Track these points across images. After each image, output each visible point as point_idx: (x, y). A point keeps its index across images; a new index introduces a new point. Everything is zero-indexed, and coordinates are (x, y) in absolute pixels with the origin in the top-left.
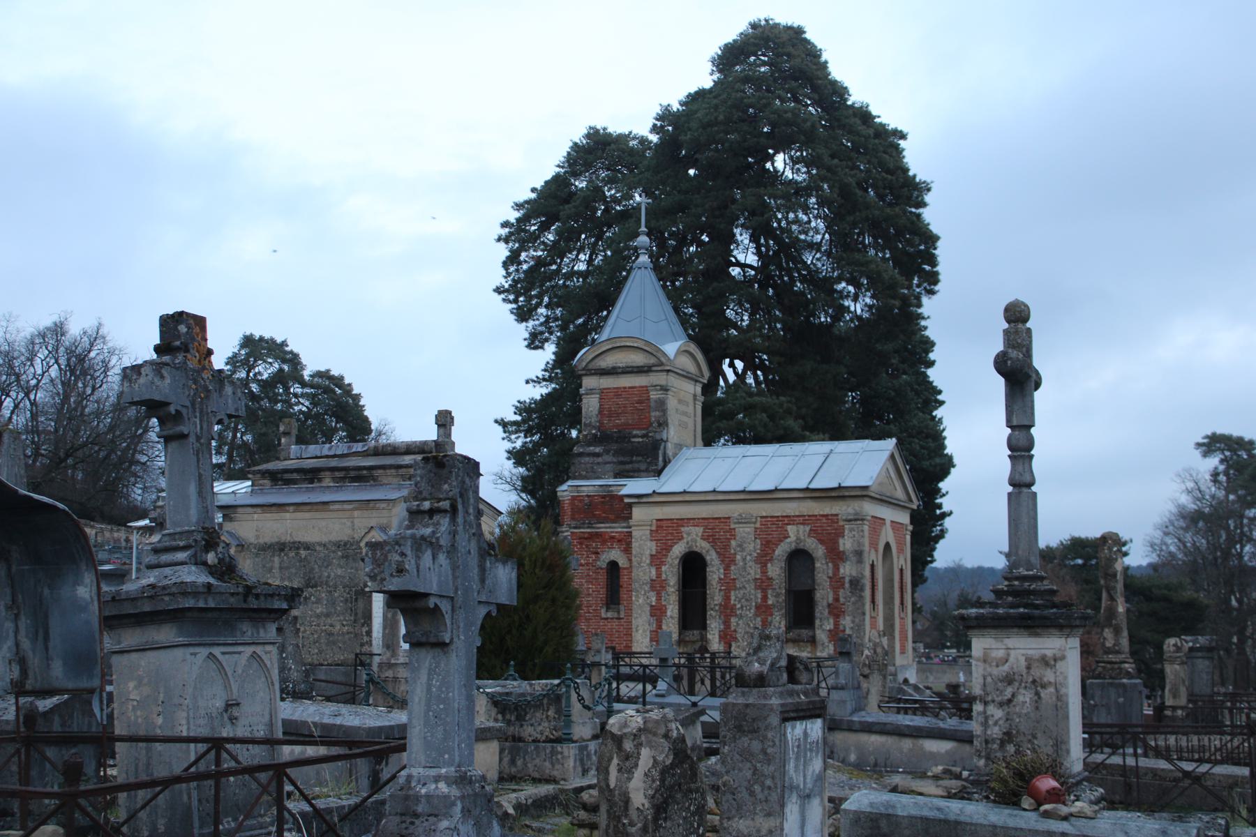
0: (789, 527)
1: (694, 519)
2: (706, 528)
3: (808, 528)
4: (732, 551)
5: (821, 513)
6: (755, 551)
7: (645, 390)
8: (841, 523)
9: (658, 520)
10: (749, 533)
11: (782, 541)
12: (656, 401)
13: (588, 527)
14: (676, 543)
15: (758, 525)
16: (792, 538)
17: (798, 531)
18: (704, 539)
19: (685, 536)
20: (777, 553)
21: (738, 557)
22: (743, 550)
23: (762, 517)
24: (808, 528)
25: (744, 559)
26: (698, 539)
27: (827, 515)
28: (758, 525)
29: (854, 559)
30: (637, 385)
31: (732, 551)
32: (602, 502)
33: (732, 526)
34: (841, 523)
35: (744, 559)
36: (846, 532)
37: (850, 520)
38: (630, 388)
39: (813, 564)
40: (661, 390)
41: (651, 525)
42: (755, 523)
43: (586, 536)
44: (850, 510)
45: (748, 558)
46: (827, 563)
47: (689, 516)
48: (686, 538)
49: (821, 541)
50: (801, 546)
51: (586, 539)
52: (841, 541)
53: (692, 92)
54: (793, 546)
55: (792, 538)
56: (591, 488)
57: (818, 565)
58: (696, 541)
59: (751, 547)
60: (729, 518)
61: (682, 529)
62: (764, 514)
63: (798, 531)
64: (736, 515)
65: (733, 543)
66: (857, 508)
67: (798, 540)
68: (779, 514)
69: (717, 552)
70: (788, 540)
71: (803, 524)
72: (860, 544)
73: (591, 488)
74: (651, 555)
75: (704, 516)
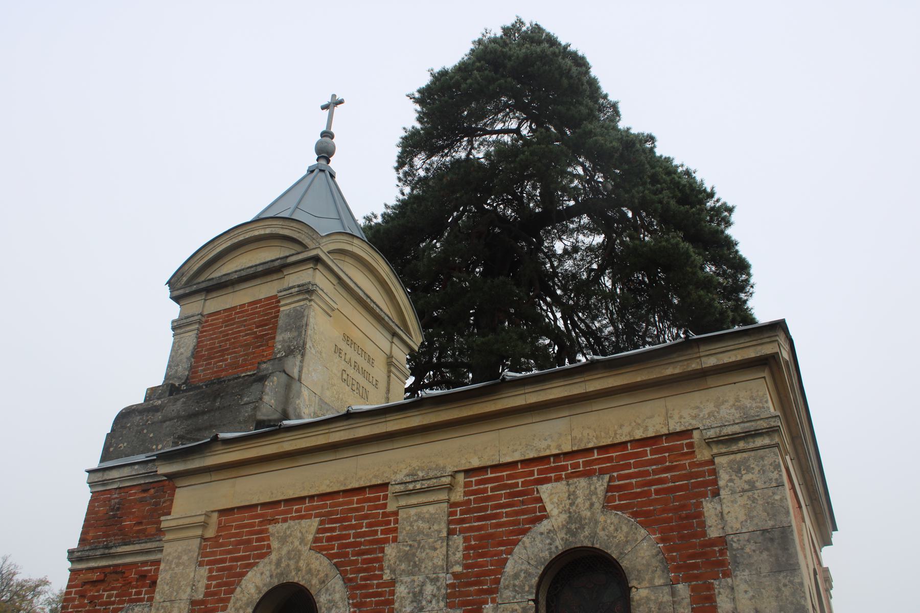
0: (545, 491)
1: (301, 499)
2: (326, 518)
3: (600, 484)
4: (387, 576)
5: (639, 434)
6: (447, 569)
7: (273, 303)
8: (703, 454)
9: (223, 512)
10: (431, 520)
11: (524, 532)
12: (288, 315)
13: (103, 557)
14: (251, 566)
15: (458, 495)
16: (556, 516)
17: (572, 496)
18: (319, 550)
19: (275, 544)
20: (509, 568)
21: (401, 590)
22: (415, 568)
23: (468, 472)
24: (600, 484)
25: (417, 596)
26: (305, 549)
27: (656, 439)
28: (458, 495)
29: (763, 561)
30: (262, 296)
31: (387, 576)
32: (141, 500)
33: (391, 507)
34: (703, 454)
35: (417, 596)
36: (723, 478)
37: (732, 439)
38: (250, 304)
39: (626, 591)
40: (300, 293)
41: (205, 525)
42: (450, 488)
43: (95, 576)
44: (728, 412)
45: (429, 589)
46: (672, 583)
47: (291, 494)
48: (278, 550)
49: (646, 519)
50: (583, 539)
51: (94, 583)
52: (709, 508)
53: (698, 177)
54: (560, 545)
55: (556, 516)
56: (126, 472)
57: (640, 593)
58: (299, 553)
59: (438, 557)
60: (385, 486)
61: (271, 528)
62: (476, 463)
63: (572, 496)
64: (400, 477)
65: (391, 551)
66: (748, 403)
67: (574, 521)
68: (517, 457)
69: (346, 581)
70: (545, 526)
71: (588, 474)
72: (775, 509)
73: (126, 472)
74: (193, 603)
75: (325, 489)
